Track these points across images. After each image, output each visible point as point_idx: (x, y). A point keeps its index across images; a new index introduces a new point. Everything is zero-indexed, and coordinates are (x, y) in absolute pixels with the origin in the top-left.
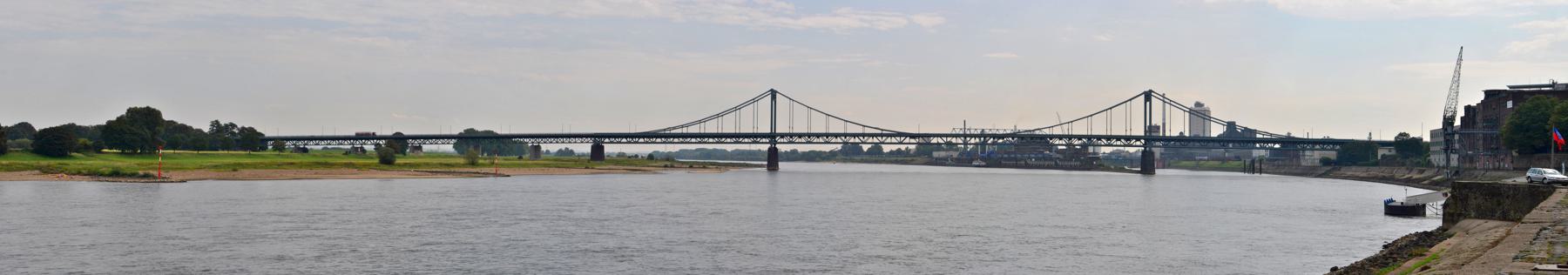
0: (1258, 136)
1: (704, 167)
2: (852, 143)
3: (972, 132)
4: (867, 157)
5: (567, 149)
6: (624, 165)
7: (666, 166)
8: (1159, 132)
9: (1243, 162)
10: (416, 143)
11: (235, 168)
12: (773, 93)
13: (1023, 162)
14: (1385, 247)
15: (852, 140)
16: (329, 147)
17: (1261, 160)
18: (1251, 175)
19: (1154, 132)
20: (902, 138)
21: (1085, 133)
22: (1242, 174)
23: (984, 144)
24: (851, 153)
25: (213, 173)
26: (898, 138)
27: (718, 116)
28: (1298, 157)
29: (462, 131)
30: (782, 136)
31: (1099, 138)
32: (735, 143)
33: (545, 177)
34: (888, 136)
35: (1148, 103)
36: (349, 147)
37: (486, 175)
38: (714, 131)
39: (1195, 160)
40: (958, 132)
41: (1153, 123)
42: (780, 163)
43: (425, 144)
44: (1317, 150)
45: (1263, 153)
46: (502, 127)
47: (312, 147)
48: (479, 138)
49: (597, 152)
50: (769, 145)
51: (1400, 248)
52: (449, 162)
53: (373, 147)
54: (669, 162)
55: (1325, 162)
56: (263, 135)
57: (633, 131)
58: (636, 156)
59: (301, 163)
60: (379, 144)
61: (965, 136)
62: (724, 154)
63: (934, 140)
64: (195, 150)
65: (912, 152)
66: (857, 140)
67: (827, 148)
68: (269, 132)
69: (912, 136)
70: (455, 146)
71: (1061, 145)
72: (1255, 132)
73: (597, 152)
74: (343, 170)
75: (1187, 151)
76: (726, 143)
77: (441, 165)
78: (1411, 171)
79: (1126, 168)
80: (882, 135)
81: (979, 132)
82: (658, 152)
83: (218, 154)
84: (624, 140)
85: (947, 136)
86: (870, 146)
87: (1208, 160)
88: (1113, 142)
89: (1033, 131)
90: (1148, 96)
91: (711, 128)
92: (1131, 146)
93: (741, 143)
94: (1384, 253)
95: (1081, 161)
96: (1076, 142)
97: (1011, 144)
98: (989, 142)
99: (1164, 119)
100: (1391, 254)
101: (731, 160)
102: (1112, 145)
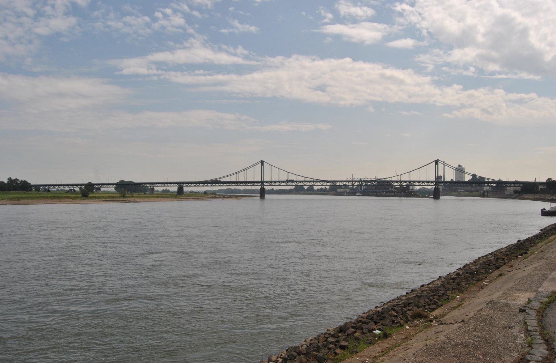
0: (486, 180)
1: (230, 197)
2: (299, 185)
3: (356, 180)
4: (306, 192)
5: (166, 189)
6: (193, 196)
7: (212, 197)
8: (441, 179)
9: (479, 193)
10: (98, 187)
11: (19, 199)
12: (262, 162)
13: (379, 194)
14: (541, 230)
15: (299, 184)
16: (59, 189)
17: (487, 191)
18: (483, 198)
19: (440, 179)
20: (323, 183)
21: (408, 180)
22: (479, 198)
23: (361, 185)
24: (299, 189)
25: (9, 202)
26: (321, 183)
27: (236, 173)
28: (504, 190)
29: (119, 182)
30: (267, 182)
31: (415, 182)
32: (244, 186)
33: (157, 202)
34: (316, 182)
35: (437, 166)
36: (68, 189)
37: (130, 201)
38: (234, 180)
39: (458, 192)
40: (349, 179)
41: (439, 175)
42: (265, 195)
43: (102, 187)
44: (512, 186)
45: (488, 188)
46: (136, 179)
47: (52, 189)
48: (126, 184)
49: (180, 190)
50: (260, 187)
51: (548, 231)
52: (113, 196)
53: (79, 189)
54: (214, 195)
55: (516, 192)
56: (30, 184)
57: (197, 181)
58: (199, 192)
59: (47, 196)
60: (81, 188)
61: (352, 181)
62: (239, 191)
63: (338, 184)
64: (1, 191)
65: (327, 189)
66: (302, 184)
67: (288, 188)
68: (33, 182)
69: (328, 182)
70: (116, 188)
71: (397, 185)
72: (485, 178)
73: (180, 190)
74: (66, 200)
75: (455, 188)
76: (241, 186)
77: (109, 197)
78: (553, 195)
79: (427, 196)
80: (313, 182)
81: (359, 180)
82: (208, 190)
83: (11, 193)
84: (193, 185)
85: (344, 181)
86: (308, 187)
87: (464, 192)
88: (421, 184)
89: (384, 179)
90: (437, 162)
91: (233, 179)
92: (429, 185)
93: (247, 186)
94: (541, 233)
95: (406, 193)
96: (404, 184)
97: (374, 185)
98: (364, 184)
99: (444, 173)
100: (544, 233)
101: (243, 194)
102: (420, 185)
